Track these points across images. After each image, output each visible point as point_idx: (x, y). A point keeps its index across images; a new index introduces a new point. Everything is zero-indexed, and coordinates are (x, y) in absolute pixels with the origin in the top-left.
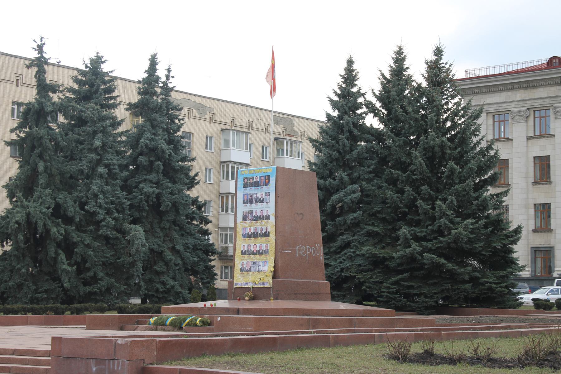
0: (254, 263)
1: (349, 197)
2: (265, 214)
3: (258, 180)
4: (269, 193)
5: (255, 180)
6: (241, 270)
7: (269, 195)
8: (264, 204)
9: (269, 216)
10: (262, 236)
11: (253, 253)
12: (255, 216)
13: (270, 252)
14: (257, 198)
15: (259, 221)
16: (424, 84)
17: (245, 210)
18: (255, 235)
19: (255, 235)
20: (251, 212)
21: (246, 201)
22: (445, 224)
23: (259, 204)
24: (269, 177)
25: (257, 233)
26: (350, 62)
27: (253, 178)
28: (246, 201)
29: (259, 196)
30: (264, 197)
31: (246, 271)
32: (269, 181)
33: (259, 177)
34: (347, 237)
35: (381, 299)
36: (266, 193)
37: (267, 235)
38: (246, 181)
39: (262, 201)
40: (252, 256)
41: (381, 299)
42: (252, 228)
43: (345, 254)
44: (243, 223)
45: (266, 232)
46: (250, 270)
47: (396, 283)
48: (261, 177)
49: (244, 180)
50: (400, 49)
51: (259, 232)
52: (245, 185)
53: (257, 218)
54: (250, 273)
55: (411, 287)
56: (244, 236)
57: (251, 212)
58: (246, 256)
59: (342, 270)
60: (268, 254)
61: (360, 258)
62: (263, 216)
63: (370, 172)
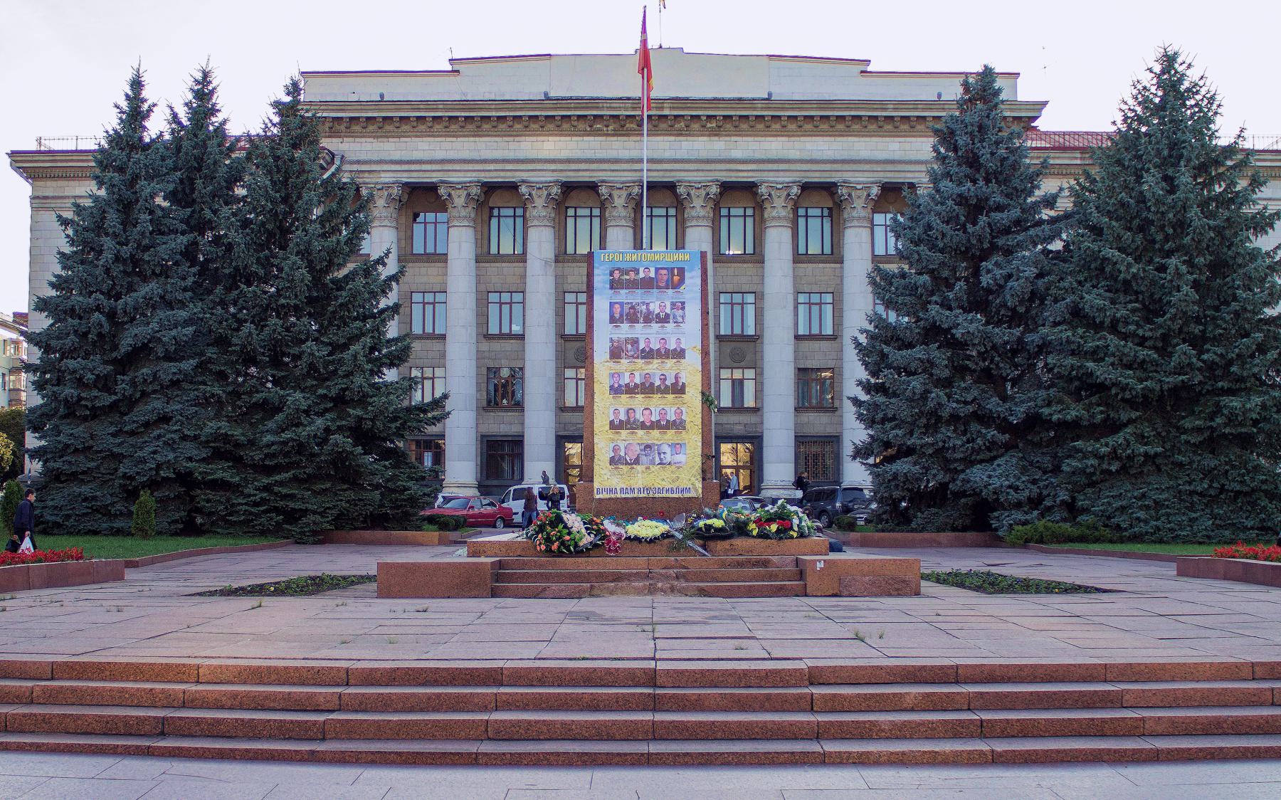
0: (648, 446)
1: (174, 333)
2: (672, 346)
3: (652, 274)
4: (683, 303)
5: (642, 275)
6: (613, 461)
7: (683, 308)
8: (670, 326)
9: (683, 351)
10: (664, 390)
11: (643, 426)
12: (643, 350)
13: (688, 426)
14: (649, 312)
15: (655, 361)
16: (106, 146)
17: (615, 337)
18: (647, 388)
19: (647, 388)
20: (635, 342)
21: (617, 316)
22: (361, 386)
23: (655, 326)
24: (681, 271)
25: (652, 384)
26: (137, 84)
27: (637, 271)
28: (617, 316)
29: (655, 308)
30: (668, 311)
31: (627, 463)
32: (682, 281)
33: (653, 270)
34: (156, 404)
35: (233, 518)
36: (673, 304)
37: (678, 389)
38: (617, 275)
39: (664, 320)
40: (640, 433)
41: (233, 518)
42: (637, 374)
43: (159, 436)
44: (611, 364)
45: (675, 384)
46: (637, 461)
47: (267, 488)
48: (657, 270)
49: (611, 274)
50: (206, 75)
51: (657, 383)
52: (614, 285)
53: (648, 355)
54: (639, 468)
55: (291, 497)
56: (615, 390)
57: (635, 342)
58: (624, 433)
59: (159, 467)
60: (684, 428)
61: (188, 444)
62: (651, 350)
63: (185, 290)
